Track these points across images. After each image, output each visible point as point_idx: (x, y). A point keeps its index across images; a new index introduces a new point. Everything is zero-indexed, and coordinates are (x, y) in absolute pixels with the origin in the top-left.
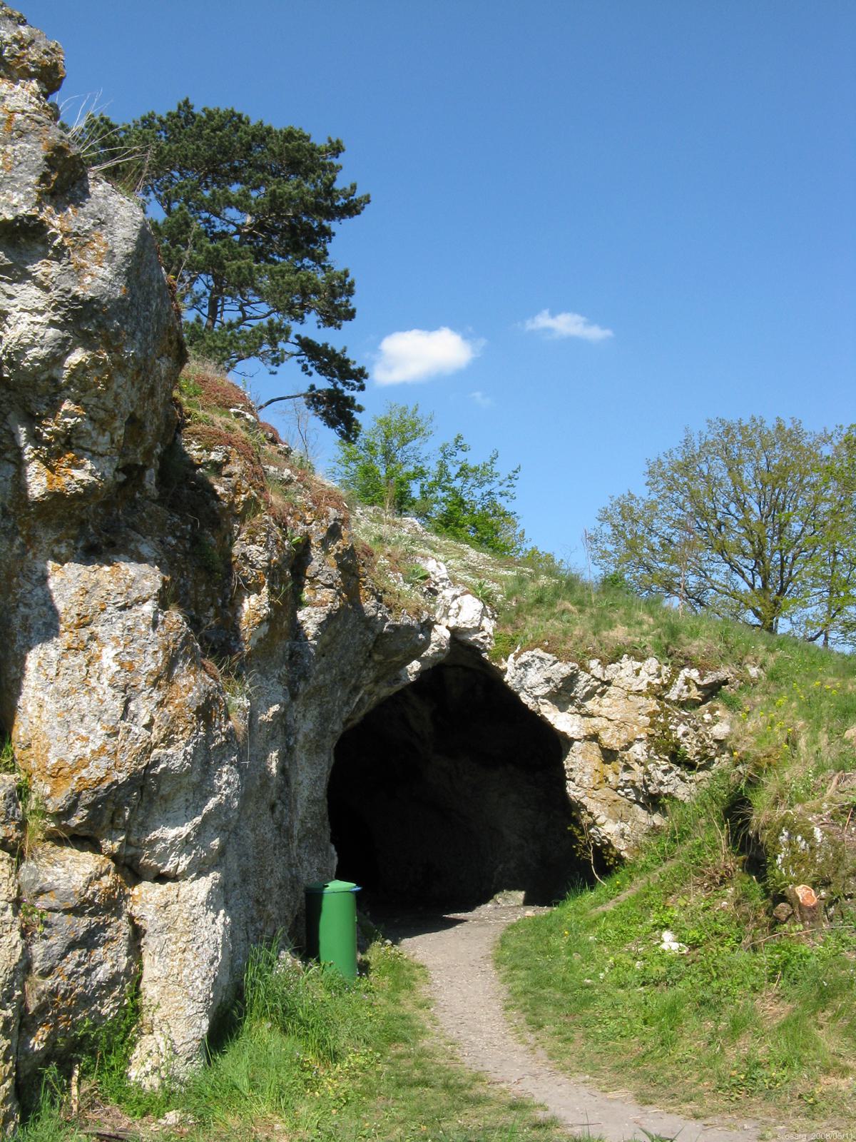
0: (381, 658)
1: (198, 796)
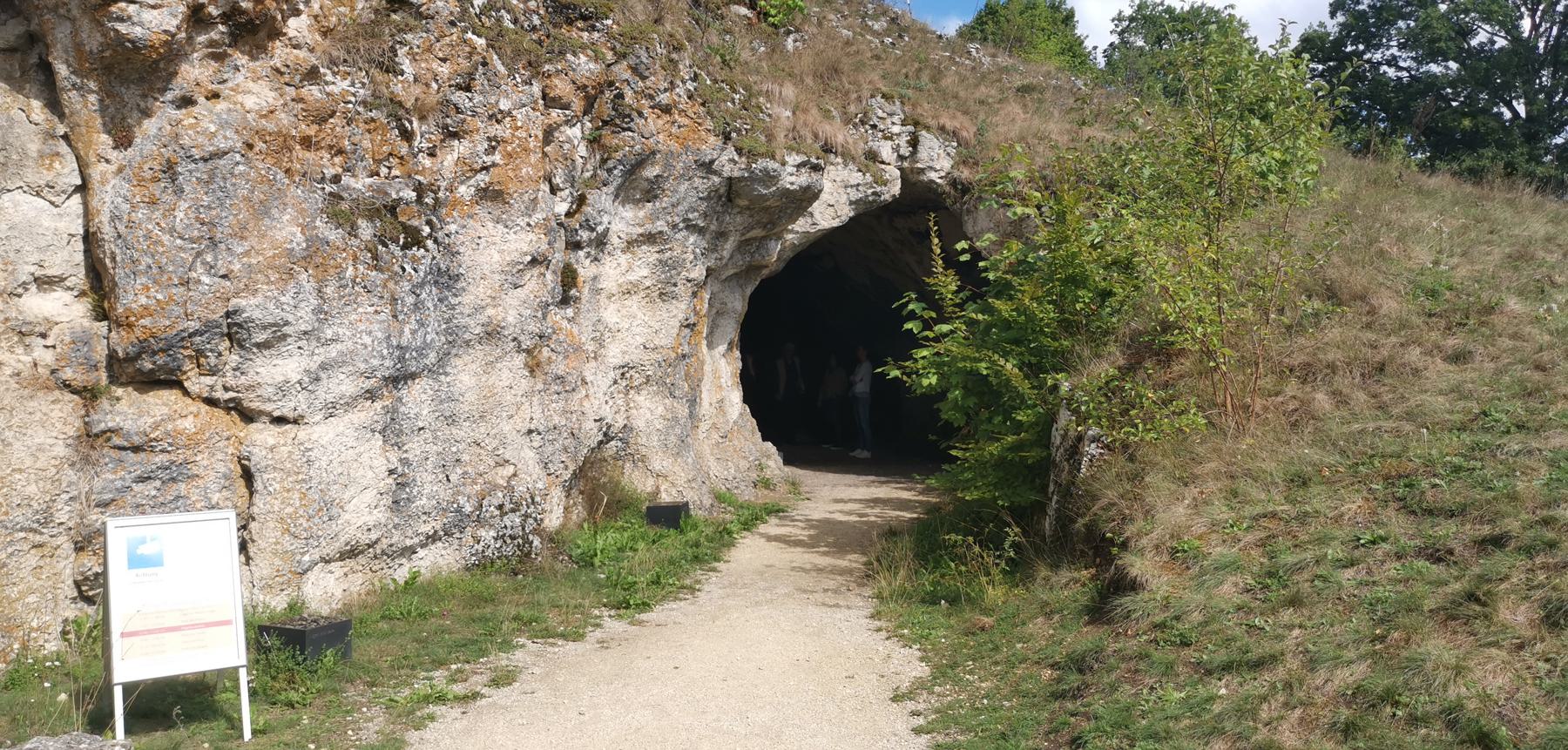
0: (747, 203)
1: (314, 343)
